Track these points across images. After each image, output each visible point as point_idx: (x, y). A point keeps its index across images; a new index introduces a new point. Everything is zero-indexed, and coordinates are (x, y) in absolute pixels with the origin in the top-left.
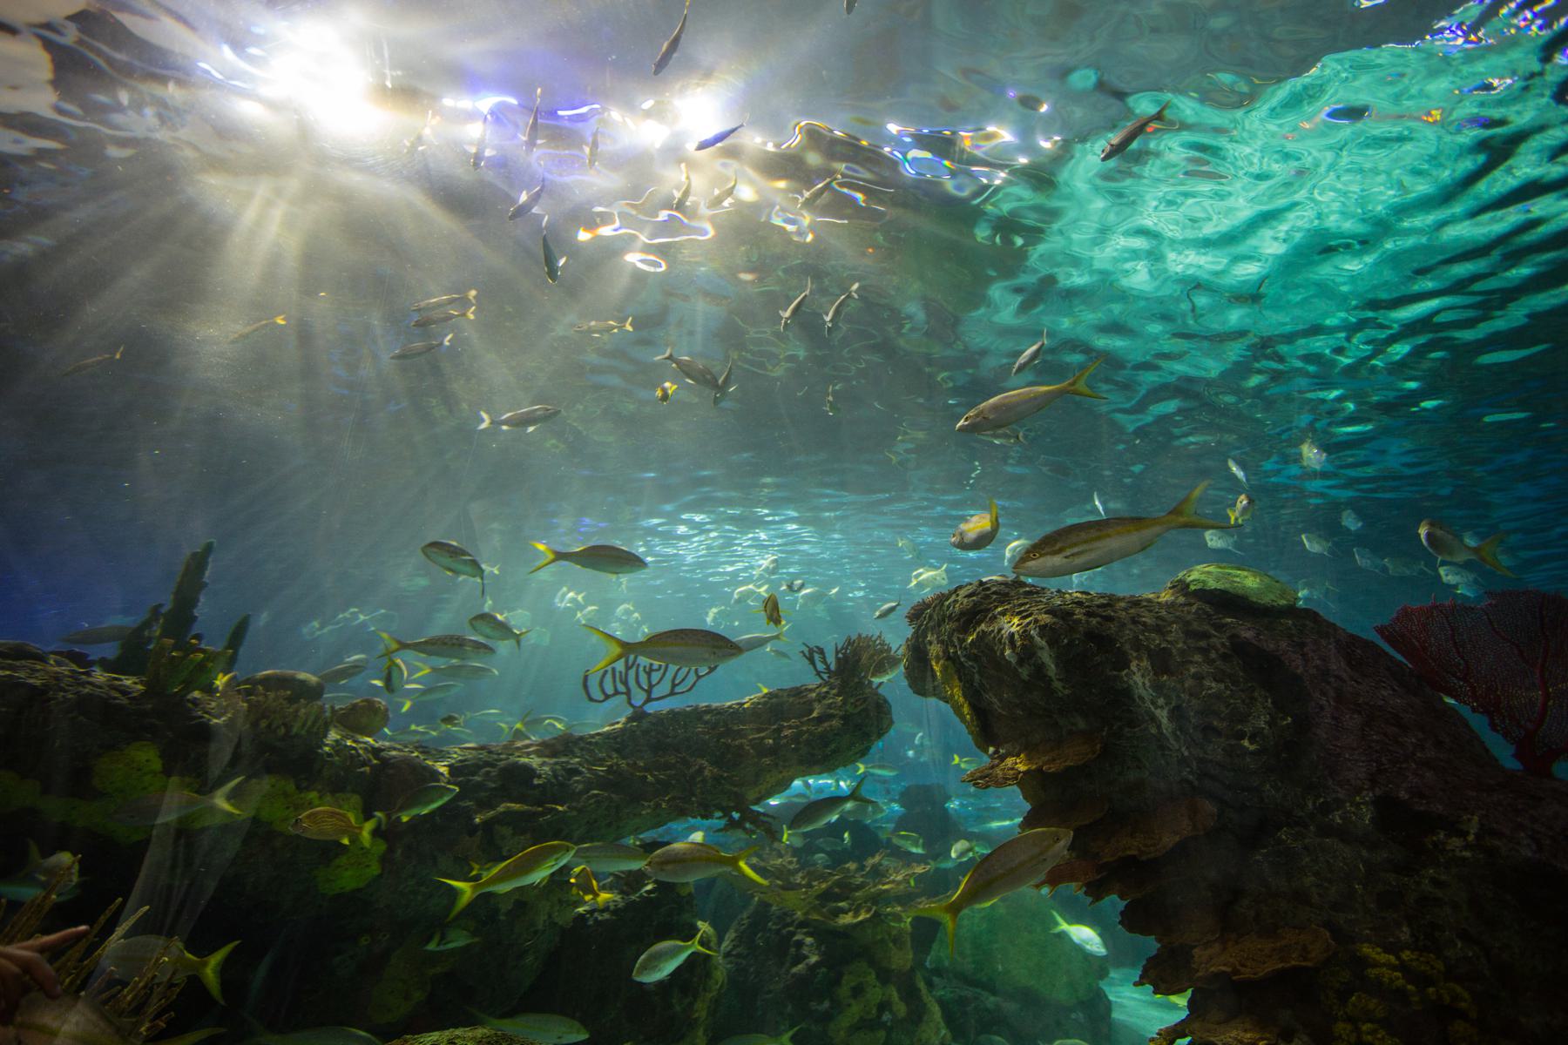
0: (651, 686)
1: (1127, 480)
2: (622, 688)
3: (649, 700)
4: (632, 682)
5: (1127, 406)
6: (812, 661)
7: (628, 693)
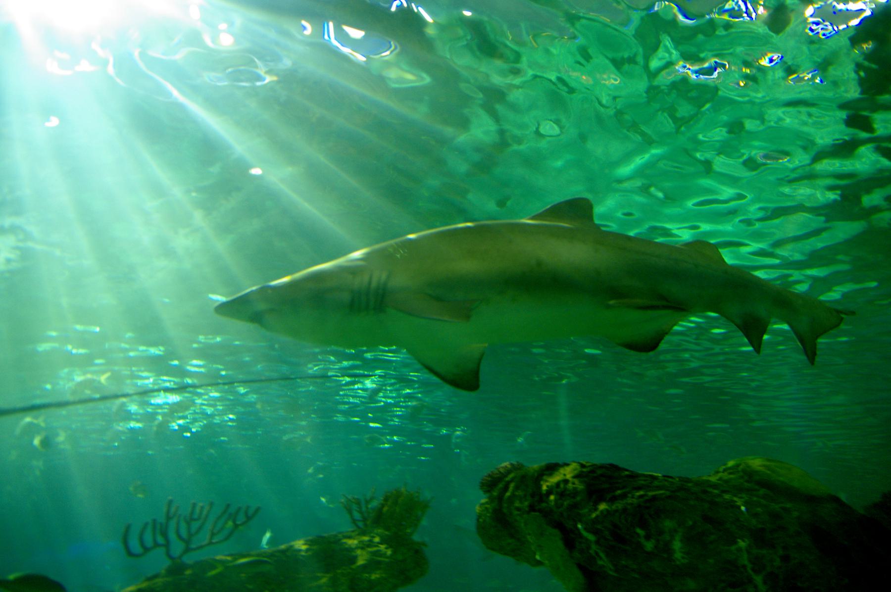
0: (190, 535)
1: (818, 81)
2: (160, 540)
3: (188, 550)
4: (172, 535)
5: (124, 400)
6: (350, 511)
7: (167, 545)
